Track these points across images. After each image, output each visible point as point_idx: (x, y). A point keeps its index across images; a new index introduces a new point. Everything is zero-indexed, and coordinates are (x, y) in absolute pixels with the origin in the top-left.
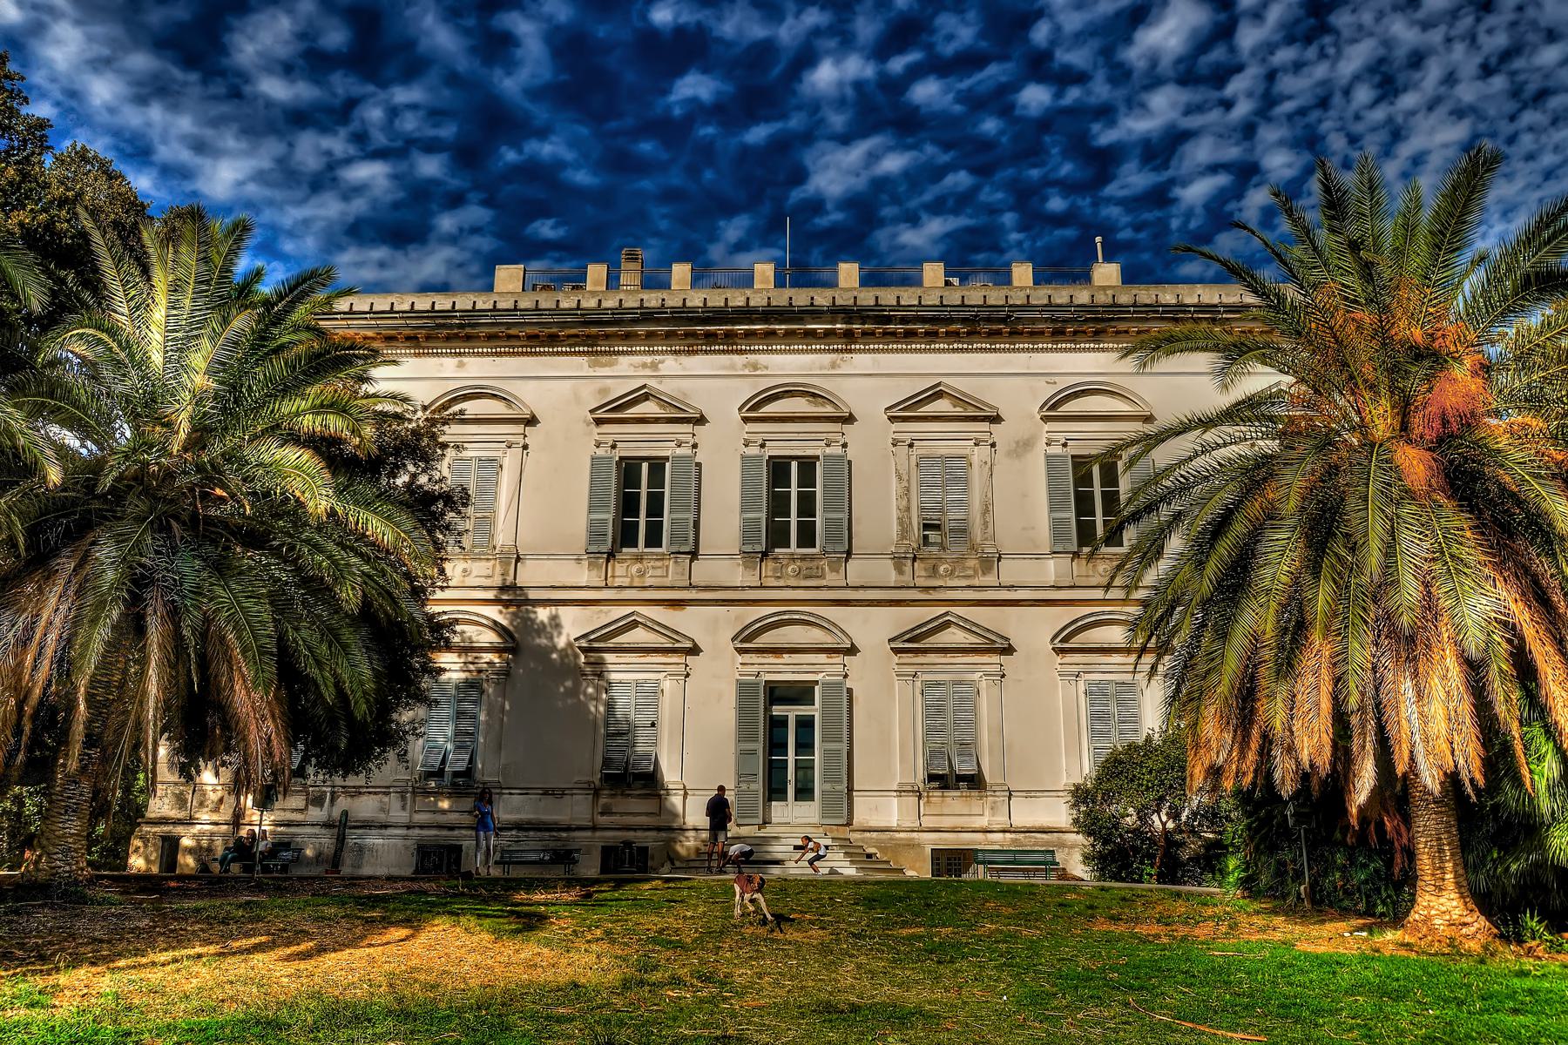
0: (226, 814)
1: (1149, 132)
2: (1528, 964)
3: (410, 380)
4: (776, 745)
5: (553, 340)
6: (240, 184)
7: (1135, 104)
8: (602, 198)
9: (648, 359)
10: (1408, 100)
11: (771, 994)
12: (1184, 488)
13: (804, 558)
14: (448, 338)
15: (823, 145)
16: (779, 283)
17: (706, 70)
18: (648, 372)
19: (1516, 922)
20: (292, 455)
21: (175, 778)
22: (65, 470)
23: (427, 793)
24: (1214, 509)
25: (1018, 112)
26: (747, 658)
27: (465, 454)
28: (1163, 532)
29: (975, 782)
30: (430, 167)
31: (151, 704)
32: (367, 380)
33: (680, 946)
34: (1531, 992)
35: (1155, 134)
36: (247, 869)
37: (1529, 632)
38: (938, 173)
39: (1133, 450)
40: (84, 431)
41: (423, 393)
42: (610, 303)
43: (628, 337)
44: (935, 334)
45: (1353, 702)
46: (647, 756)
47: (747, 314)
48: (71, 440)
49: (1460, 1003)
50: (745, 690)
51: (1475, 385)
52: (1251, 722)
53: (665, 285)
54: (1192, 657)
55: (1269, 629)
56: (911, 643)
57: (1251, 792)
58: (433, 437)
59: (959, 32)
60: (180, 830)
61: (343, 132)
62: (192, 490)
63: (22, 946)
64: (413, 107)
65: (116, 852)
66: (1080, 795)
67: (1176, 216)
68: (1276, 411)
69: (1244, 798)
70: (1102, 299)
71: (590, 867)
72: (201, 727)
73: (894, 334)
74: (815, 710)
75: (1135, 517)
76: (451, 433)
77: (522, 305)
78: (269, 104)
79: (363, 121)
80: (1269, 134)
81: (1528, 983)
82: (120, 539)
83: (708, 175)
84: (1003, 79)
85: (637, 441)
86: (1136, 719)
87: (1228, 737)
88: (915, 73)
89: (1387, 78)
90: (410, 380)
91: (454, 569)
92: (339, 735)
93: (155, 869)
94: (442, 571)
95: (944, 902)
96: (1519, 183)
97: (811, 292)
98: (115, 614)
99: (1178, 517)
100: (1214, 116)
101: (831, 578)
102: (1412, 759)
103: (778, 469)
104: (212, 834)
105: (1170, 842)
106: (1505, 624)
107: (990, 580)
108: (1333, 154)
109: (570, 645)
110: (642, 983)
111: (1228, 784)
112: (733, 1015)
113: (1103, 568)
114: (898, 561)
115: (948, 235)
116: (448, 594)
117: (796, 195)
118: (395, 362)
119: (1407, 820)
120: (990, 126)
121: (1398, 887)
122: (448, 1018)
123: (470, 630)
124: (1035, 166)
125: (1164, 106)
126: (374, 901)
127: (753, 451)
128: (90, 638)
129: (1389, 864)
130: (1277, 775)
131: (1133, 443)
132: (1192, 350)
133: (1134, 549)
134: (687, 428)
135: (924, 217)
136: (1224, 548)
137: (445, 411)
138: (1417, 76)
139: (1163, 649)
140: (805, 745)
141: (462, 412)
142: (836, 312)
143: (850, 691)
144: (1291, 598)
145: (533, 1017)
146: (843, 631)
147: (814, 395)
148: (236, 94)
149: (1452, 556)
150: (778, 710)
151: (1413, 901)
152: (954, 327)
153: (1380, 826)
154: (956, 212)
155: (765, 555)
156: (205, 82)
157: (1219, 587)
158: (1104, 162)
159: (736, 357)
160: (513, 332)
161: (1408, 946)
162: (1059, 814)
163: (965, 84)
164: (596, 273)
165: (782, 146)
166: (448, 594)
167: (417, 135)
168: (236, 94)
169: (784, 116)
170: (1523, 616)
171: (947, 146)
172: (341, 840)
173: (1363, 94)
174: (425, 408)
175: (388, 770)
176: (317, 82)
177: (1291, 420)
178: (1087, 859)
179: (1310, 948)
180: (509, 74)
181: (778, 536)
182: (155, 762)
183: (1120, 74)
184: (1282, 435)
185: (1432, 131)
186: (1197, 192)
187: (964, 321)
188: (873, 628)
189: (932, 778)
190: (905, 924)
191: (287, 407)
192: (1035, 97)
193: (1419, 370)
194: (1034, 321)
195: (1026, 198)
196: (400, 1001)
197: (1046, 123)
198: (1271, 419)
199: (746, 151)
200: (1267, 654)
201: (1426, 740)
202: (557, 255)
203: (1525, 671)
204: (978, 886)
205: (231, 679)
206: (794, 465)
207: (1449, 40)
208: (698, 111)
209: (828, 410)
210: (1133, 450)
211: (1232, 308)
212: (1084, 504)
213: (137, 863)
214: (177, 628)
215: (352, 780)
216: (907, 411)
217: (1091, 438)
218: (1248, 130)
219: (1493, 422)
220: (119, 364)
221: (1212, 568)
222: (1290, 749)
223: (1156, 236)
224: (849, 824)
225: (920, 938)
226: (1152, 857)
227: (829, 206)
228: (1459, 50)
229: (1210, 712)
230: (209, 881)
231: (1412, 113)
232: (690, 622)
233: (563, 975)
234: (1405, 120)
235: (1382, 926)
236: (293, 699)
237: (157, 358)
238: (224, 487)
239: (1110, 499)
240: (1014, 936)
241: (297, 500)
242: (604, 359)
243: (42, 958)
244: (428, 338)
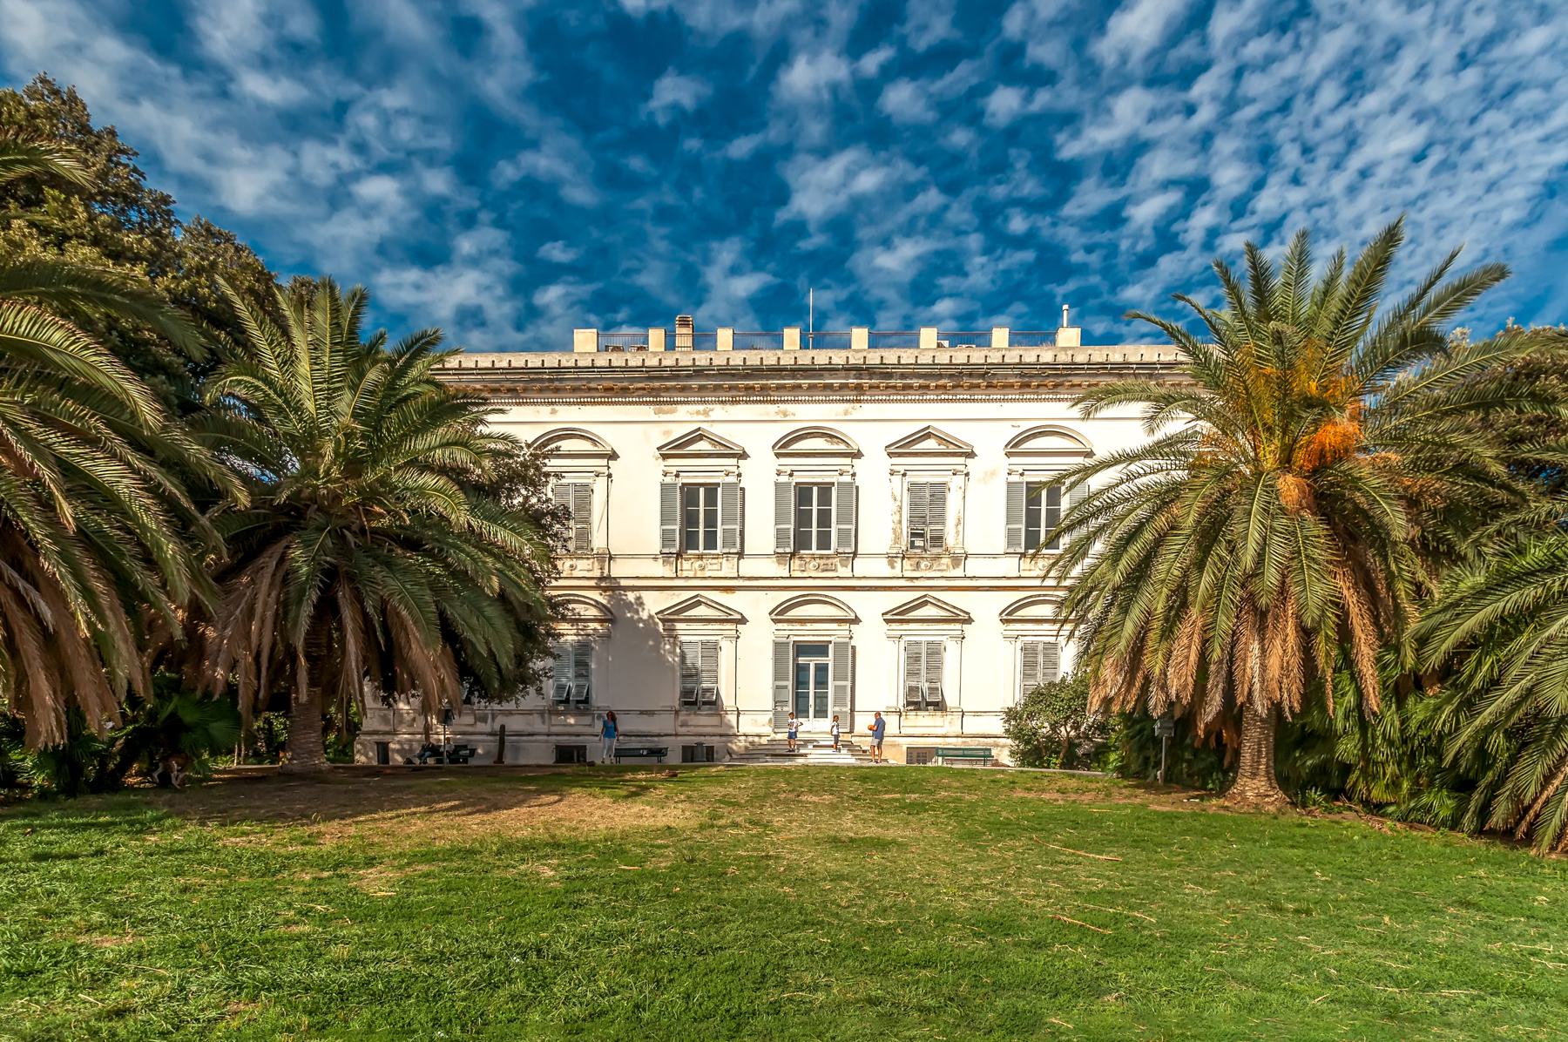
0: (419, 725)
1: (1113, 142)
2: (1308, 820)
3: (520, 423)
4: (800, 682)
5: (625, 391)
6: (260, 199)
7: (1101, 111)
8: (605, 217)
9: (701, 407)
10: (1371, 102)
11: (796, 832)
12: (1109, 507)
13: (821, 557)
14: (541, 390)
15: (803, 159)
16: (804, 345)
17: (682, 71)
18: (702, 418)
19: (1303, 794)
20: (429, 480)
21: (379, 705)
22: (251, 493)
23: (559, 713)
24: (1131, 522)
25: (986, 121)
26: (780, 626)
27: (563, 481)
28: (1090, 539)
29: (939, 706)
30: (437, 182)
31: (353, 658)
32: (482, 422)
33: (738, 804)
34: (1305, 836)
35: (1118, 146)
36: (440, 761)
37: (1354, 610)
38: (910, 191)
39: (1073, 479)
40: (263, 462)
41: (527, 435)
42: (669, 361)
43: (683, 389)
44: (927, 387)
45: (1215, 656)
46: (709, 690)
47: (777, 371)
48: (253, 470)
49: (1255, 841)
50: (779, 647)
51: (1352, 428)
52: (1138, 669)
54: (1100, 625)
55: (1160, 607)
56: (897, 616)
57: (1131, 714)
58: (537, 468)
59: (933, 26)
60: (387, 738)
61: (343, 141)
62: (356, 508)
63: (290, 809)
64: (403, 112)
65: (345, 751)
66: (1011, 714)
67: (1128, 237)
68: (1189, 448)
69: (1127, 718)
70: (1063, 358)
71: (674, 758)
72: (390, 673)
73: (894, 387)
74: (829, 660)
75: (1070, 528)
76: (553, 464)
77: (598, 363)
78: (261, 106)
79: (359, 129)
80: (1225, 145)
81: (1305, 831)
82: (307, 545)
83: (698, 193)
84: (974, 80)
85: (697, 471)
86: (1055, 665)
87: (1120, 679)
88: (889, 73)
89: (1355, 78)
90: (520, 423)
91: (564, 565)
92: (483, 679)
93: (375, 763)
94: (555, 567)
95: (917, 784)
96: (1461, 195)
97: (830, 353)
98: (314, 598)
99: (1102, 529)
100: (1174, 123)
101: (844, 571)
102: (1250, 693)
103: (803, 492)
104: (410, 741)
105: (1071, 744)
106: (1337, 604)
107: (959, 572)
108: (1284, 167)
109: (651, 617)
110: (712, 826)
111: (1115, 708)
112: (773, 844)
113: (1043, 563)
114: (891, 559)
115: (919, 258)
116: (561, 583)
117: (782, 216)
118: (502, 411)
119: (1239, 732)
120: (960, 138)
121: (1225, 773)
122: (586, 847)
123: (579, 608)
124: (999, 182)
125: (1129, 110)
126: (529, 780)
128: (297, 616)
129: (1221, 760)
130: (1152, 703)
131: (1075, 473)
132: (1130, 400)
133: (1066, 550)
134: (733, 461)
135: (897, 240)
136: (1135, 550)
137: (546, 446)
138: (1388, 70)
139: (1082, 619)
140: (821, 682)
141: (558, 449)
142: (848, 369)
143: (854, 648)
144: (1180, 586)
145: (642, 845)
148: (223, 94)
149: (1307, 556)
150: (802, 660)
151: (1234, 781)
152: (942, 382)
153: (1219, 736)
154: (926, 233)
155: (793, 555)
156: (186, 76)
157: (1128, 578)
158: (1064, 176)
159: (770, 407)
160: (593, 385)
161: (1227, 808)
162: (997, 726)
163: (938, 86)
164: (656, 336)
165: (765, 160)
166: (561, 583)
167: (414, 145)
168: (223, 94)
169: (762, 126)
170: (1351, 598)
171: (918, 161)
172: (502, 742)
173: (1329, 94)
174: (529, 446)
175: (530, 700)
176: (302, 80)
177: (1200, 455)
178: (1012, 754)
179: (1158, 808)
180: (490, 73)
181: (802, 541)
182: (362, 694)
183: (1090, 72)
184: (1191, 467)
185: (1391, 135)
186: (1147, 212)
187: (951, 376)
188: (870, 607)
189: (909, 703)
190: (886, 792)
191: (420, 444)
192: (1004, 102)
193: (1309, 416)
194: (1006, 377)
195: (989, 216)
196: (553, 837)
197: (1013, 133)
198: (1184, 454)
199: (731, 165)
200: (1156, 625)
201: (1263, 681)
202: (571, 279)
203: (1345, 634)
204: (937, 770)
205: (408, 641)
206: (815, 489)
207: (1433, 21)
208: (685, 121)
209: (842, 447)
210: (1073, 479)
211: (1169, 365)
212: (1033, 518)
213: (360, 759)
214: (363, 609)
215: (506, 706)
216: (901, 449)
217: (1041, 471)
218: (1205, 140)
219: (1361, 456)
220: (280, 410)
221: (1123, 564)
222: (1164, 687)
223: (1106, 258)
224: (851, 731)
225: (897, 800)
226: (1058, 753)
227: (812, 228)
228: (1439, 39)
229: (1108, 662)
230: (412, 770)
231: (1374, 116)
232: (735, 601)
233: (661, 821)
234: (1366, 125)
235: (1210, 796)
236: (457, 653)
237: (310, 405)
238: (381, 504)
239: (1053, 516)
240: (959, 800)
241: (441, 515)
243: (304, 816)
244: (525, 390)
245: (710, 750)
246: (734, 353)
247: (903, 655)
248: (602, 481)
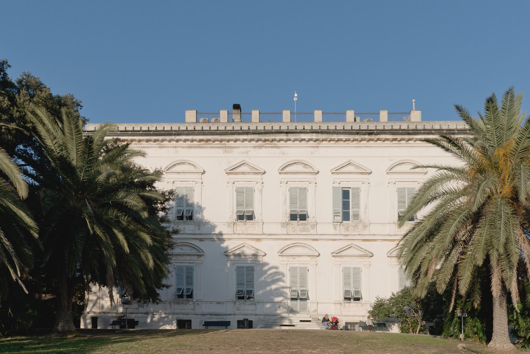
9: (245, 150)
47: (217, 133)
56: (337, 254)
85: (243, 181)
101: (312, 232)
107: (366, 232)
127: (336, 185)
146: (316, 250)
189: (346, 299)
209: (310, 170)
242: (228, 150)
245: (251, 322)
246: (260, 124)
247: (342, 274)
248: (259, 186)
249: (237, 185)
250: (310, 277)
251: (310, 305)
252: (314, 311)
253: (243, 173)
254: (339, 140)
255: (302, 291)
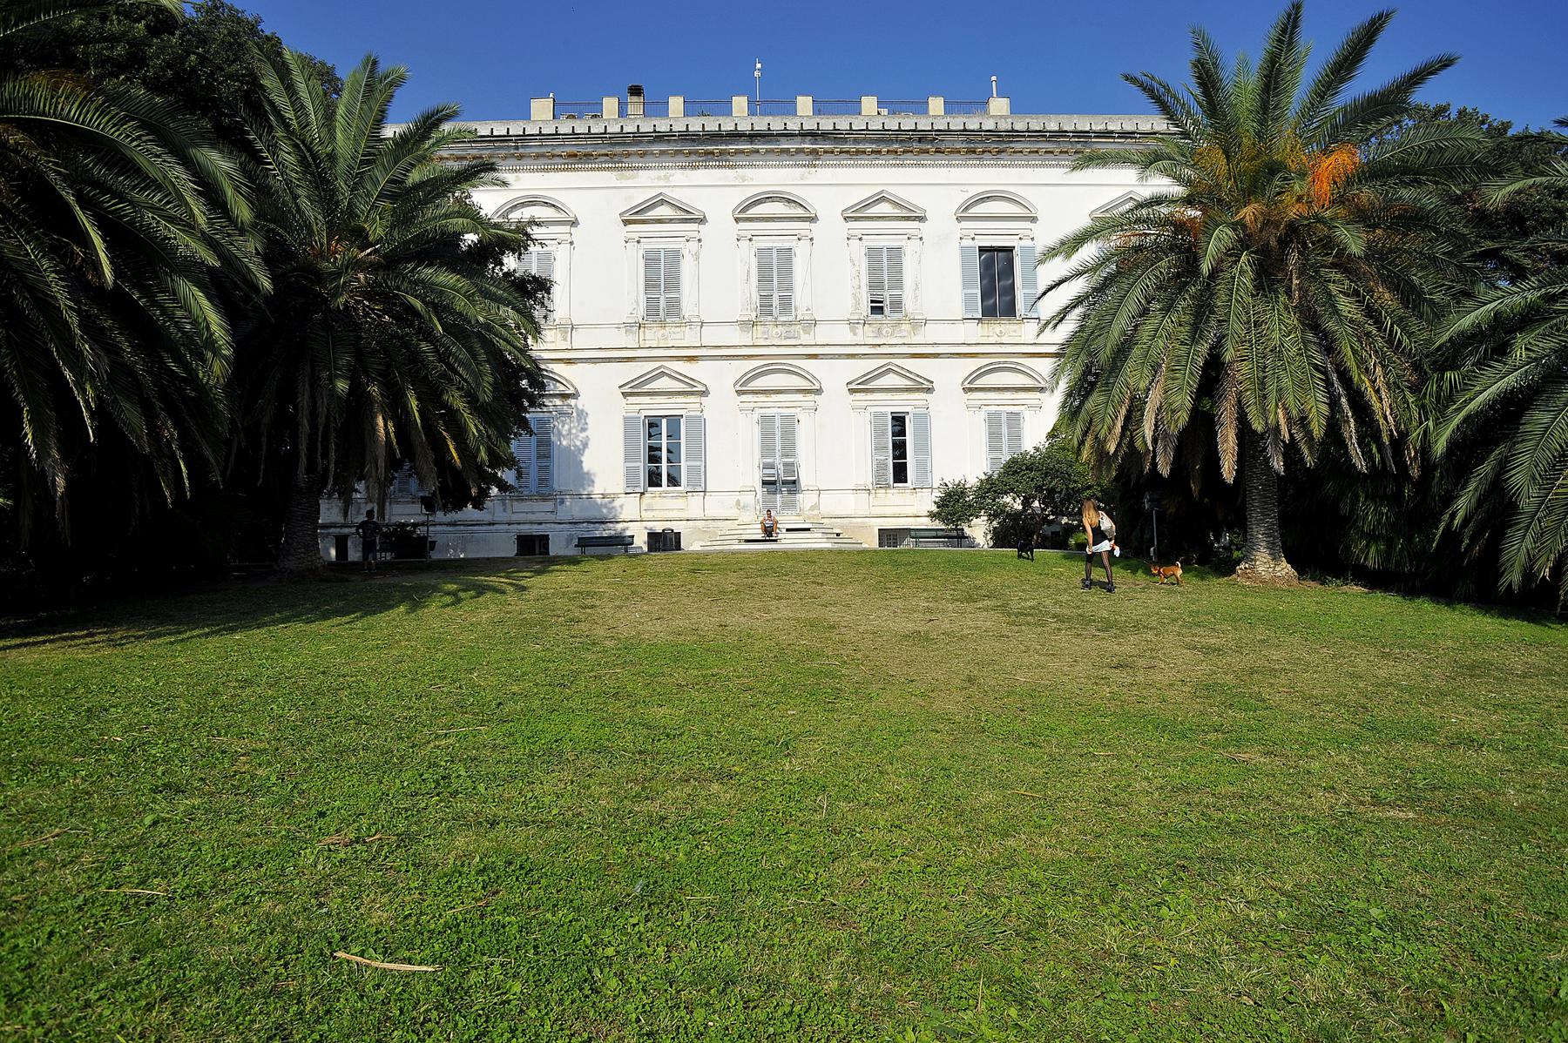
9: (662, 173)
53: (664, 113)
56: (859, 387)
127: (967, 242)
142: (804, 134)
147: (789, 201)
209: (799, 212)
248: (693, 245)
249: (647, 245)
250: (802, 434)
251: (805, 500)
252: (813, 508)
253: (659, 221)
254: (858, 152)
255: (785, 465)
